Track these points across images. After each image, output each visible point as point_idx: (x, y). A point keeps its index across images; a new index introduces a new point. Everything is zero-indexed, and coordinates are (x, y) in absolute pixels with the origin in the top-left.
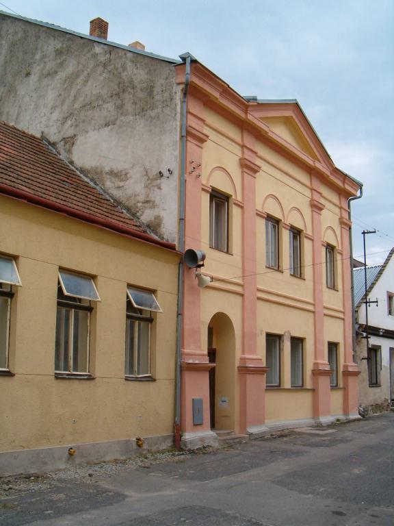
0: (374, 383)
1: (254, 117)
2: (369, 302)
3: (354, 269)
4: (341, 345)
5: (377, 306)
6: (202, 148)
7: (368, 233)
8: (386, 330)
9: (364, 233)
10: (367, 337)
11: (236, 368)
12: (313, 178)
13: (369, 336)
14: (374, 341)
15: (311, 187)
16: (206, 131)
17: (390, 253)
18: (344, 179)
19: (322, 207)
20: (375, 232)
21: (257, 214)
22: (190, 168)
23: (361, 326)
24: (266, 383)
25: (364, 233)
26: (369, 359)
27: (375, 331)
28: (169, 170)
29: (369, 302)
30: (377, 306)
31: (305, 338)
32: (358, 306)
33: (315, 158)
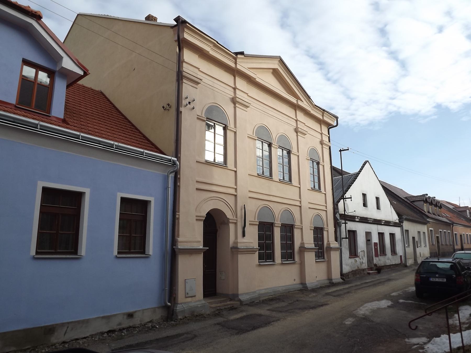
0: (354, 253)
1: (243, 65)
2: (346, 198)
3: (334, 178)
4: (86, 194)
5: (351, 200)
6: (197, 88)
7: (343, 150)
8: (374, 219)
9: (340, 151)
10: (345, 223)
11: (230, 248)
12: (237, 78)
13: (347, 222)
14: (351, 226)
15: (234, 86)
16: (200, 75)
17: (363, 165)
18: (323, 113)
19: (199, 81)
20: (348, 150)
21: (198, 118)
22: (184, 102)
23: (341, 215)
24: (315, 258)
25: (340, 151)
26: (349, 238)
27: (352, 219)
28: (169, 105)
29: (346, 198)
30: (351, 200)
31: (85, 193)
32: (338, 201)
33: (298, 98)
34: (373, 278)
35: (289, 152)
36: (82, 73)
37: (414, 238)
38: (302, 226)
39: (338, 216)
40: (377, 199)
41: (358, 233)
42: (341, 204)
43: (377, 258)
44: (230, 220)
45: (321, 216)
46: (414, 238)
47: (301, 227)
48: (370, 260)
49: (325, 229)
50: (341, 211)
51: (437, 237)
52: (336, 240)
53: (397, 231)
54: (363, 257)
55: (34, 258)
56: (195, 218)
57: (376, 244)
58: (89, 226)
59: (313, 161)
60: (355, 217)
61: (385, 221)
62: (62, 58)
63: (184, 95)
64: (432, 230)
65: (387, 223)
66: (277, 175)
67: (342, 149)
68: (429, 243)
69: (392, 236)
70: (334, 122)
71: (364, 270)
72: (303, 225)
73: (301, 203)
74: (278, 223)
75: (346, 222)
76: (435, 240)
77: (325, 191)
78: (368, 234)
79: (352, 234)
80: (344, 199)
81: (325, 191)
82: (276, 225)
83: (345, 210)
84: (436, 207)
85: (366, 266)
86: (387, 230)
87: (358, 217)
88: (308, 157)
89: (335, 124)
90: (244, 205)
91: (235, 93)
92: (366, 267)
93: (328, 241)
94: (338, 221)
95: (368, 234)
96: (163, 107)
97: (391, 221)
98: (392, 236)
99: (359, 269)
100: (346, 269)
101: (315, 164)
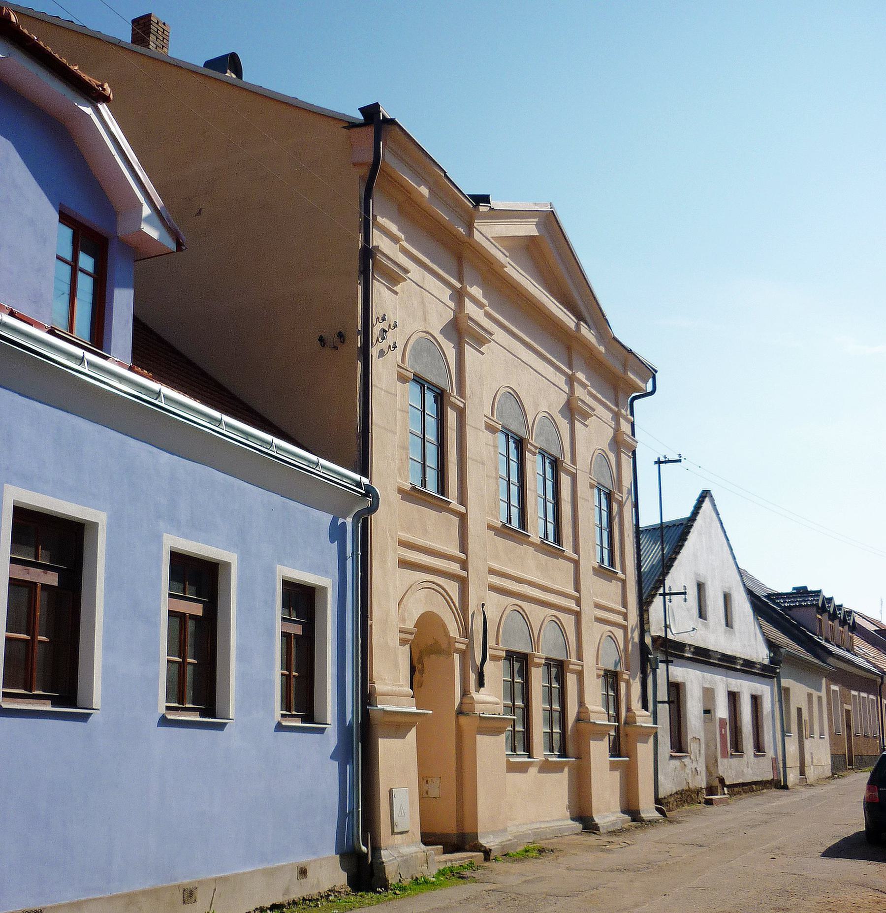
5: (685, 600)
14: (680, 672)
20: (679, 461)
23: (655, 639)
30: (685, 600)
34: (552, 843)
35: (521, 444)
36: (172, 246)
37: (799, 710)
38: (582, 666)
39: (648, 640)
40: (727, 598)
41: (688, 687)
42: (656, 606)
43: (725, 761)
44: (624, 675)
45: (524, 615)
46: (799, 710)
47: (580, 668)
48: (711, 765)
49: (571, 667)
50: (656, 629)
51: (848, 712)
52: (645, 707)
53: (765, 690)
54: (698, 756)
55: (164, 722)
56: (398, 636)
57: (722, 721)
58: (238, 647)
59: (600, 489)
60: (684, 645)
61: (745, 660)
62: (142, 205)
63: (376, 311)
64: (837, 691)
65: (748, 668)
66: (537, 528)
67: (662, 459)
68: (830, 727)
69: (756, 700)
70: (646, 382)
71: (698, 791)
72: (585, 663)
73: (578, 604)
74: (540, 655)
75: (669, 659)
76: (843, 720)
77: (576, 550)
78: (709, 694)
79: (676, 690)
80: (664, 595)
81: (576, 550)
82: (571, 667)
83: (667, 626)
84: (833, 621)
85: (702, 780)
86: (746, 687)
87: (690, 645)
88: (495, 419)
89: (650, 389)
90: (483, 605)
91: (460, 304)
92: (704, 785)
93: (581, 703)
94: (650, 656)
95: (709, 694)
96: (321, 339)
97: (738, 655)
98: (756, 700)
99: (689, 790)
100: (667, 787)
101: (430, 397)
